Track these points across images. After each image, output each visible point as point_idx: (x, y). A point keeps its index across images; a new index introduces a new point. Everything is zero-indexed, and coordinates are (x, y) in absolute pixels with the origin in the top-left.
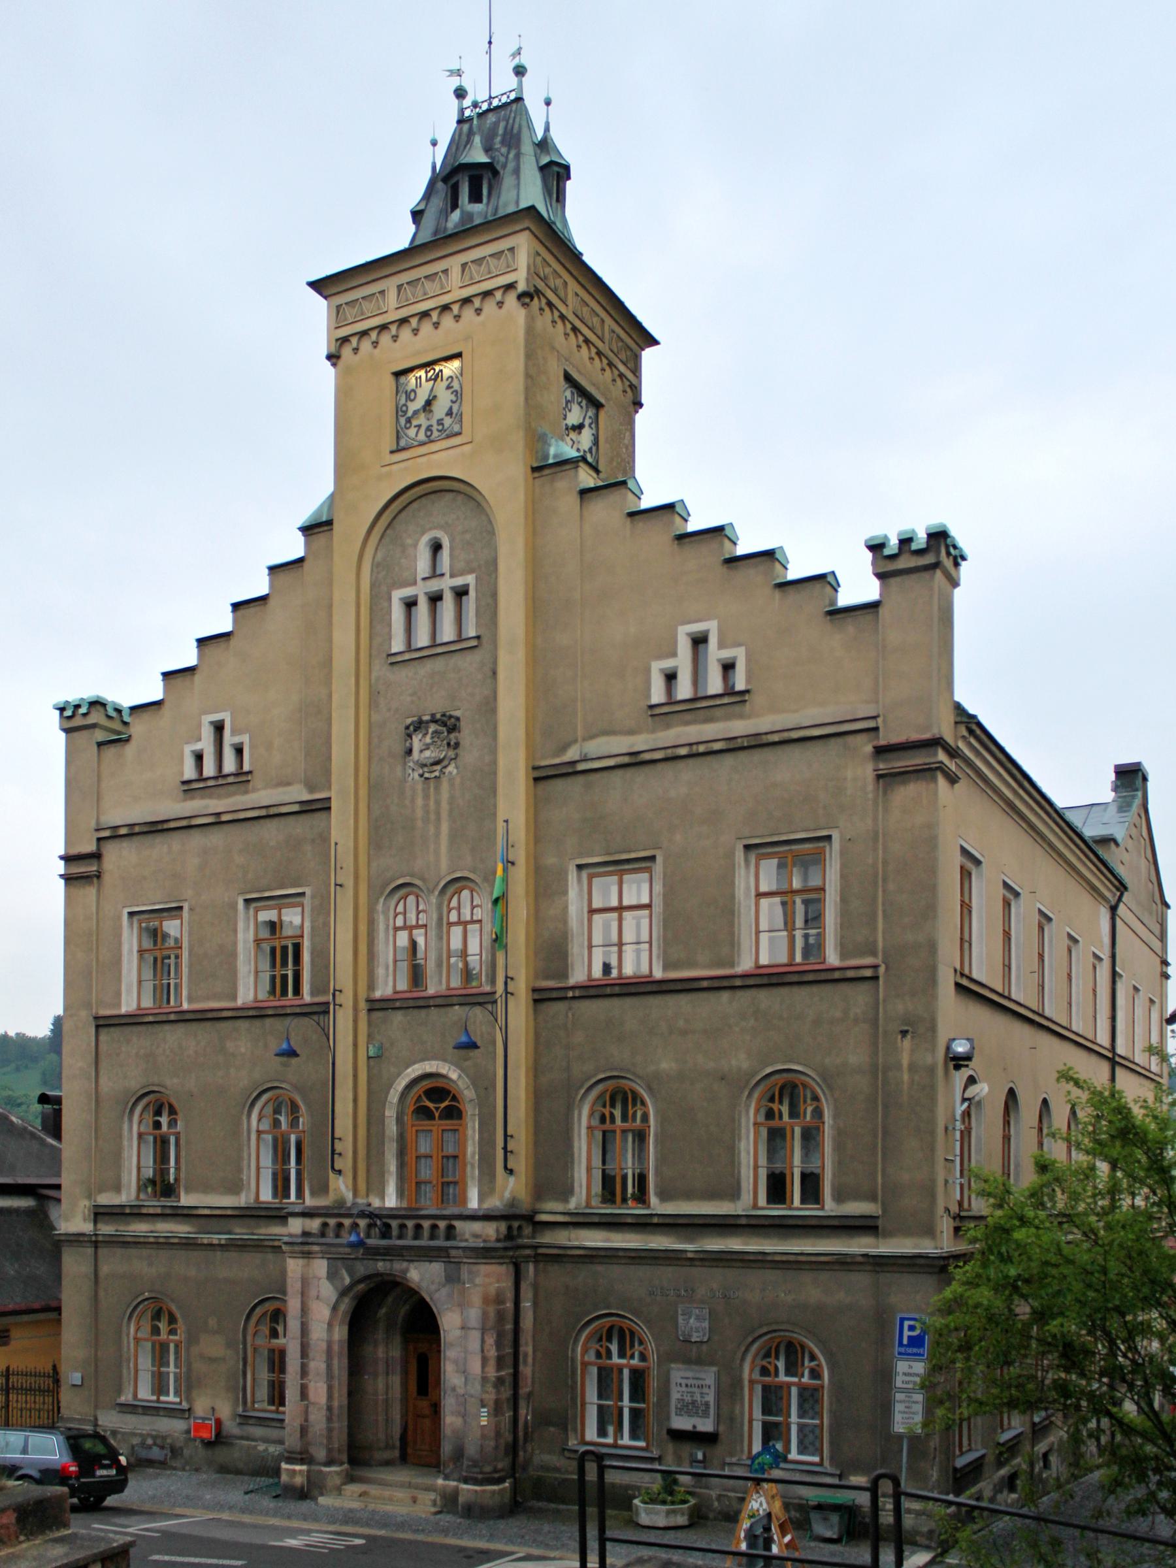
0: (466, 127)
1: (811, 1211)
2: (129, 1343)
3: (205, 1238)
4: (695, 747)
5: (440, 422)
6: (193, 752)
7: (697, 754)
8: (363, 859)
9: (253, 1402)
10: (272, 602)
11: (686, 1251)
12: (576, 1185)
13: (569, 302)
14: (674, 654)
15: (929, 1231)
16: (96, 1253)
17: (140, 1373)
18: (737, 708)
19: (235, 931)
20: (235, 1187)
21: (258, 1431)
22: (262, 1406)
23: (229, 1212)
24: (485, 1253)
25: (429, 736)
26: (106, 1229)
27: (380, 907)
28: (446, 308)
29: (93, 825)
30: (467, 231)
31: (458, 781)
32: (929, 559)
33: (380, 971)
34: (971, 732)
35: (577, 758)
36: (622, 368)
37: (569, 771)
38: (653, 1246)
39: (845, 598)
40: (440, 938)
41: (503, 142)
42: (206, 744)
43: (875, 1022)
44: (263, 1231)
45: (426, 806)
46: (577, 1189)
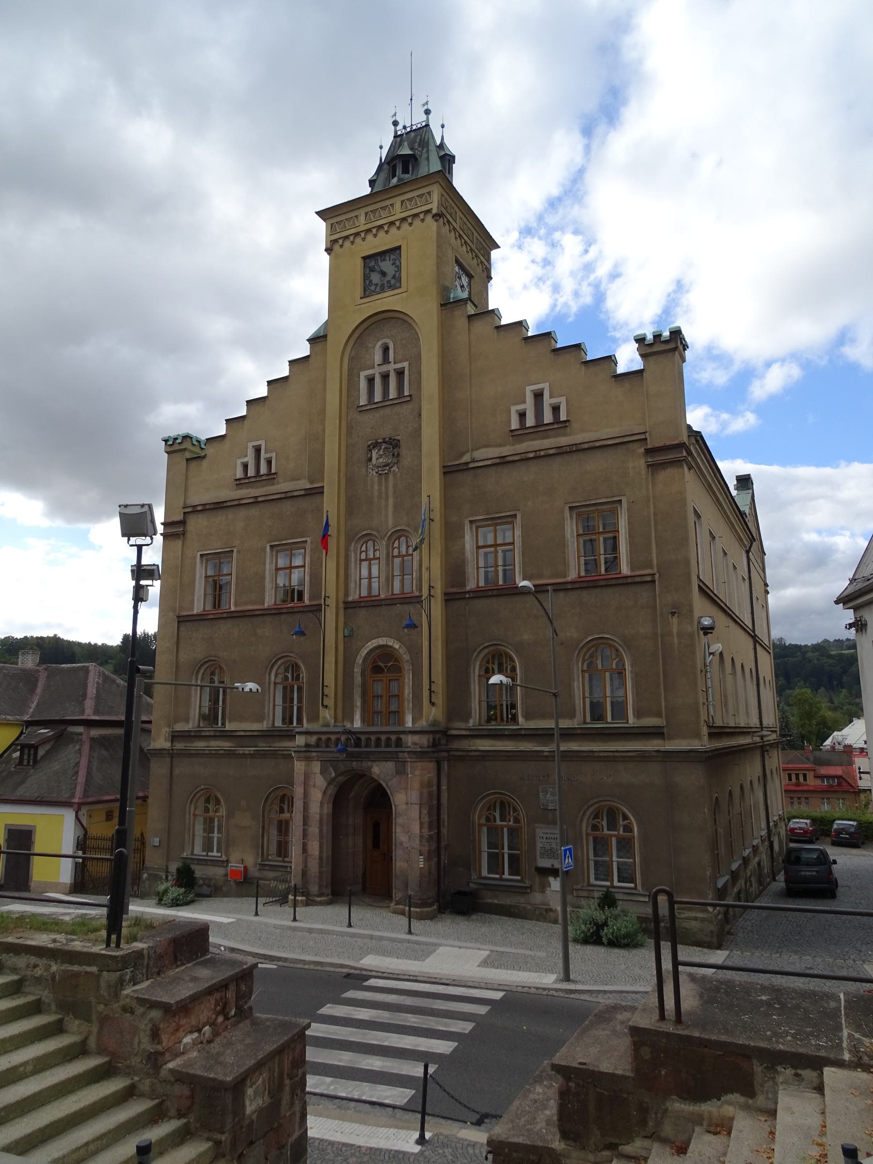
0: (398, 139)
2: (190, 818)
3: (241, 750)
4: (538, 453)
5: (389, 282)
6: (242, 463)
7: (539, 457)
8: (342, 521)
9: (268, 855)
11: (543, 751)
12: (473, 711)
13: (458, 221)
14: (524, 402)
15: (698, 735)
16: (172, 762)
17: (196, 837)
19: (264, 564)
20: (260, 719)
21: (271, 874)
22: (274, 859)
23: (256, 733)
24: (420, 755)
25: (382, 450)
26: (179, 746)
27: (352, 548)
28: (392, 223)
29: (182, 504)
30: (401, 184)
31: (399, 475)
32: (671, 346)
33: (352, 585)
34: (697, 441)
35: (469, 460)
36: (482, 258)
37: (464, 468)
38: (522, 748)
39: (621, 369)
40: (388, 565)
41: (419, 145)
42: (250, 459)
43: (654, 608)
44: (277, 745)
45: (380, 490)
46: (473, 714)
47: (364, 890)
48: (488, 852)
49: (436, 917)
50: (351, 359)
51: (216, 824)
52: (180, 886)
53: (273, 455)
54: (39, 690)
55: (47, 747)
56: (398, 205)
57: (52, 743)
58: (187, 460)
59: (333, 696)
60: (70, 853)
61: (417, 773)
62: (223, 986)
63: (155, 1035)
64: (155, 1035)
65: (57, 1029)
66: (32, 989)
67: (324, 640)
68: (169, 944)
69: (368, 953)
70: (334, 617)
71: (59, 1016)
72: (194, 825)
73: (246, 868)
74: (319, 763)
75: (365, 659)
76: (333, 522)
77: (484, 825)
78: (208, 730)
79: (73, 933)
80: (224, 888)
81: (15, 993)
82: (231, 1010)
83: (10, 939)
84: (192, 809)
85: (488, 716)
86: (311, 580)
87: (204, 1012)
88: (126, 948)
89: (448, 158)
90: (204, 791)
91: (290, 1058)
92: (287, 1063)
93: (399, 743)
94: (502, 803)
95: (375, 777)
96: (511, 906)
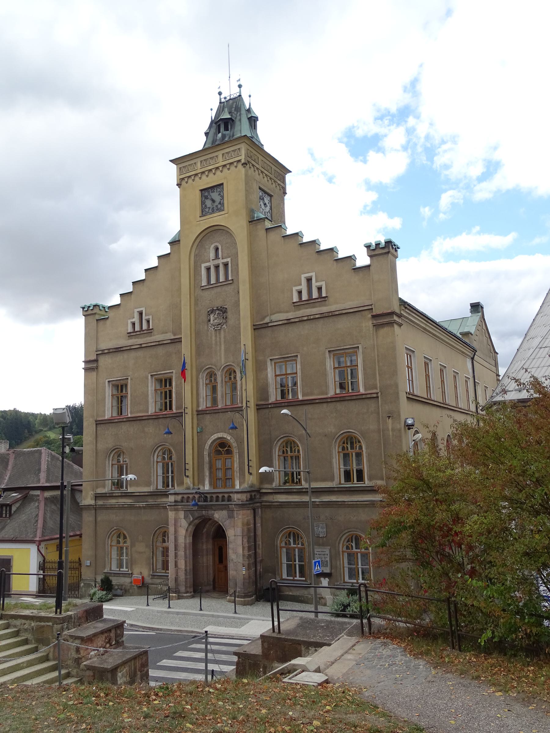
0: (222, 104)
1: (360, 484)
2: (108, 548)
3: (138, 504)
4: (309, 317)
7: (310, 319)
9: (156, 569)
10: (159, 269)
12: (275, 478)
14: (301, 285)
16: (96, 512)
18: (323, 303)
19: (148, 387)
20: (149, 484)
21: (158, 581)
22: (160, 572)
23: (146, 494)
24: (242, 506)
26: (100, 502)
27: (200, 376)
28: (217, 168)
29: (95, 349)
32: (386, 250)
33: (201, 400)
35: (269, 321)
36: (279, 182)
37: (266, 326)
41: (235, 110)
42: (136, 319)
43: (378, 414)
44: (159, 500)
45: (216, 339)
47: (214, 589)
48: (287, 564)
49: (254, 604)
50: (196, 256)
51: (125, 551)
52: (103, 590)
53: (150, 317)
54: (10, 467)
55: (17, 505)
56: (220, 157)
57: (20, 502)
58: (97, 320)
59: (191, 469)
60: (36, 573)
61: (240, 517)
62: (109, 630)
63: (78, 650)
64: (78, 650)
65: (36, 650)
66: (24, 634)
67: (185, 435)
68: (84, 613)
69: (209, 625)
70: (191, 420)
71: (35, 645)
72: (111, 550)
73: (143, 578)
74: (183, 512)
75: (210, 446)
76: (188, 361)
77: (284, 547)
78: (117, 492)
79: (41, 609)
80: (130, 590)
81: (16, 636)
82: (113, 642)
83: (12, 613)
84: (109, 542)
85: (285, 480)
86: (176, 397)
87: (101, 641)
88: (64, 614)
89: (253, 118)
90: (117, 530)
91: (140, 662)
92: (138, 665)
93: (229, 499)
94: (294, 533)
95: (216, 520)
96: (299, 596)
